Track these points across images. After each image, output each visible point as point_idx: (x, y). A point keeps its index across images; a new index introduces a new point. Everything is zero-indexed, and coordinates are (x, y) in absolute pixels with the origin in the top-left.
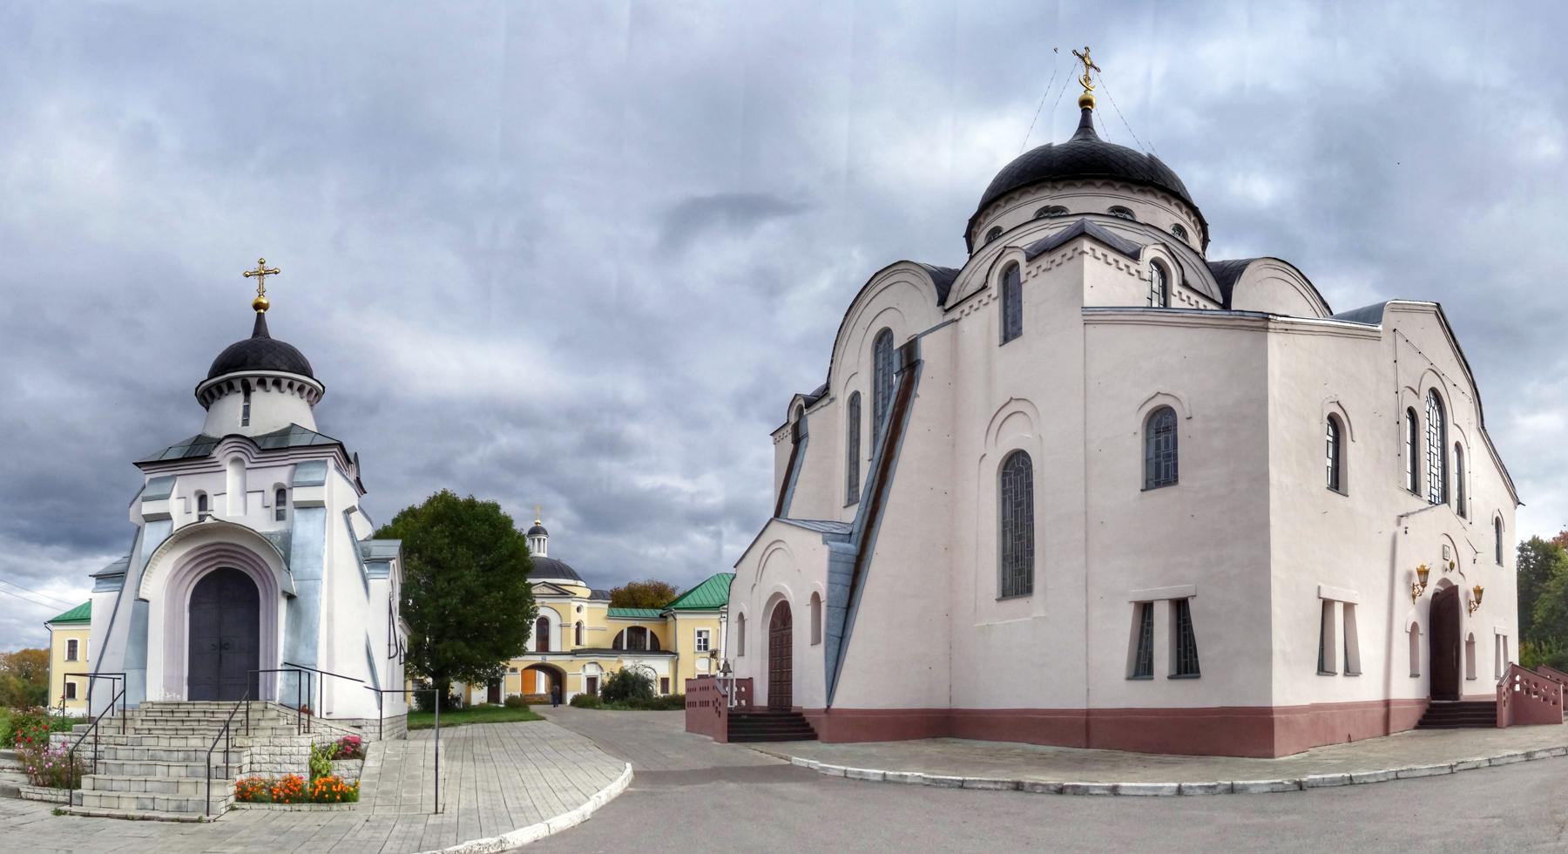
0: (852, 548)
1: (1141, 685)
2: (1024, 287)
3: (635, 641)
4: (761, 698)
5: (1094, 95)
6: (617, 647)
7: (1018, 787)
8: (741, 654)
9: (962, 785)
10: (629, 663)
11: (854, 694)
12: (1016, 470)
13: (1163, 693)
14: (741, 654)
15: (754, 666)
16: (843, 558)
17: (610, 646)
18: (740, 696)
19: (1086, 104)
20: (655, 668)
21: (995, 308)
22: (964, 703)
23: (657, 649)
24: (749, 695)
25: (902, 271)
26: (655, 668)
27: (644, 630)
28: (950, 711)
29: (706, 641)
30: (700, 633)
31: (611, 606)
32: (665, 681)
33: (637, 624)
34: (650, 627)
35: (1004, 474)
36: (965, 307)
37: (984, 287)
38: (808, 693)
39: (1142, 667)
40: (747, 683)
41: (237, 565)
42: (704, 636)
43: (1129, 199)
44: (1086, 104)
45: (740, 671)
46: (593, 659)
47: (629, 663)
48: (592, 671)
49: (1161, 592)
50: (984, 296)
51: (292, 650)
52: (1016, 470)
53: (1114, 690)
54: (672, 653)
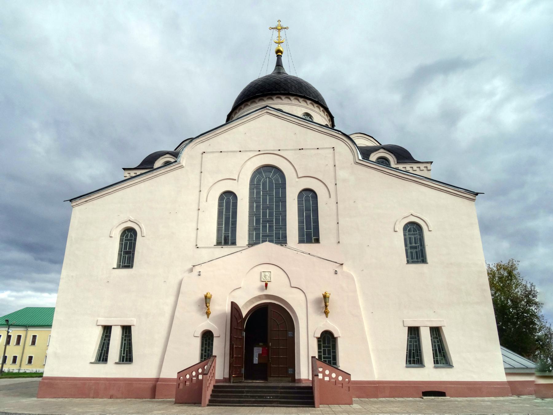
13: (112, 370)
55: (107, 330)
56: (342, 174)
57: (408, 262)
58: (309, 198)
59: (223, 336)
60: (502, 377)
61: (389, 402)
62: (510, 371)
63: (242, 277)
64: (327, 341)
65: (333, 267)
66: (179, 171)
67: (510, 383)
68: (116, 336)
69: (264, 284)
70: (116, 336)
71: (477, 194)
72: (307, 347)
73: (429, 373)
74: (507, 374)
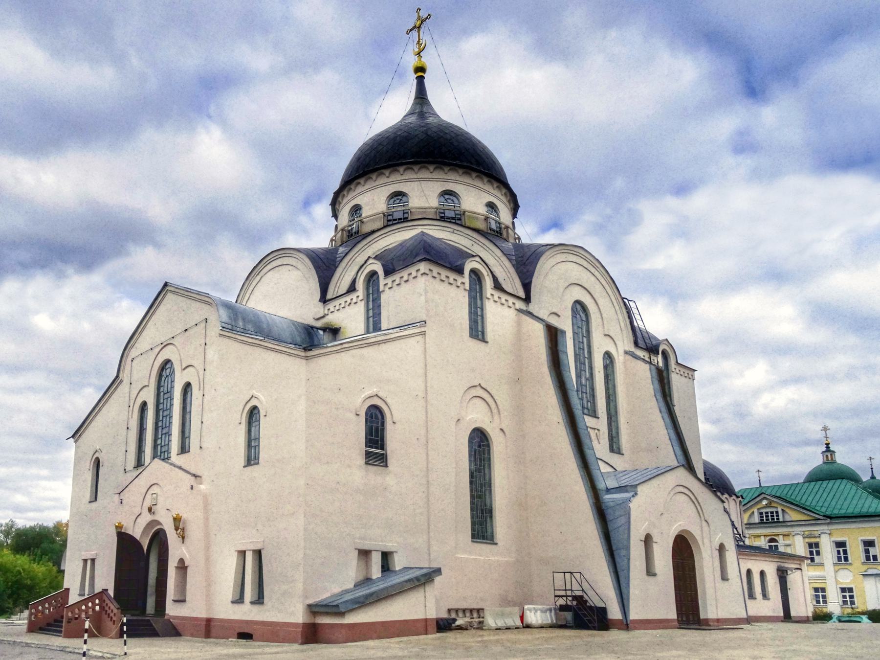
13: (247, 613)
39: (239, 600)
49: (249, 546)
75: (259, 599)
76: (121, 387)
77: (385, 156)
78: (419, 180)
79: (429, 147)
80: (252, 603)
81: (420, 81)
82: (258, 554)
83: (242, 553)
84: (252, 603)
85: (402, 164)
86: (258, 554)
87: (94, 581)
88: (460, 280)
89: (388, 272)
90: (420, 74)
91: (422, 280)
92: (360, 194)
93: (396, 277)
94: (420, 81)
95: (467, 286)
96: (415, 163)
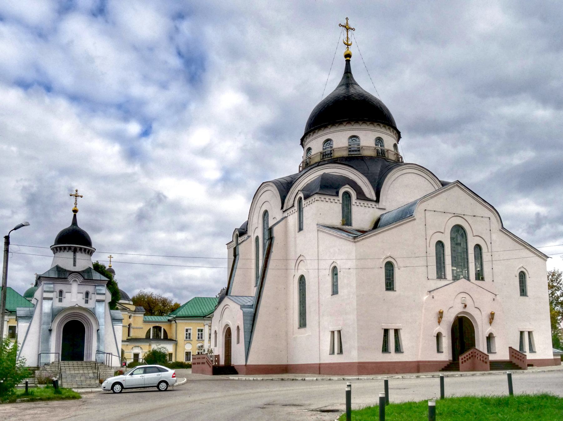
0: (252, 310)
1: (386, 355)
2: (304, 209)
3: (158, 334)
4: (222, 362)
5: (353, 50)
6: (148, 337)
7: (282, 380)
8: (216, 346)
9: (272, 380)
10: (155, 346)
11: (252, 361)
12: (302, 279)
13: (336, 359)
14: (216, 346)
15: (219, 351)
16: (250, 315)
17: (144, 337)
18: (216, 361)
19: (348, 56)
20: (169, 348)
21: (296, 215)
22: (291, 363)
23: (166, 339)
24: (218, 361)
25: (265, 186)
26: (169, 348)
27: (161, 327)
28: (287, 365)
29: (190, 334)
30: (187, 330)
31: (145, 315)
32: (171, 355)
33: (157, 325)
34: (164, 327)
35: (300, 283)
36: (288, 212)
37: (293, 206)
38: (238, 359)
39: (333, 352)
40: (218, 356)
41: (83, 322)
42: (189, 332)
43: (358, 129)
44: (348, 56)
45: (216, 353)
46: (137, 344)
47: (155, 346)
48: (136, 351)
49: (336, 329)
50: (293, 209)
51: (98, 347)
52: (302, 279)
53: (327, 358)
54: (173, 341)
55: (386, 331)
56: (494, 237)
57: (521, 295)
58: (478, 247)
59: (447, 336)
60: (552, 357)
61: (490, 374)
62: (555, 354)
63: (452, 297)
64: (490, 338)
65: (493, 296)
66: (542, 260)
67: (554, 359)
68: (392, 334)
69: (464, 305)
70: (392, 334)
71: (548, 257)
72: (115, 330)
73: (393, 357)
74: (554, 355)
75: (341, 352)
76: (412, 223)
77: (328, 115)
78: (339, 131)
79: (349, 107)
80: (338, 354)
81: (348, 62)
82: (339, 332)
83: (333, 332)
84: (338, 354)
85: (344, 121)
86: (339, 332)
87: (522, 240)
88: (338, 199)
89: (306, 197)
90: (348, 58)
91: (316, 203)
92: (309, 142)
93: (310, 199)
94: (348, 62)
95: (341, 202)
96: (368, 121)
